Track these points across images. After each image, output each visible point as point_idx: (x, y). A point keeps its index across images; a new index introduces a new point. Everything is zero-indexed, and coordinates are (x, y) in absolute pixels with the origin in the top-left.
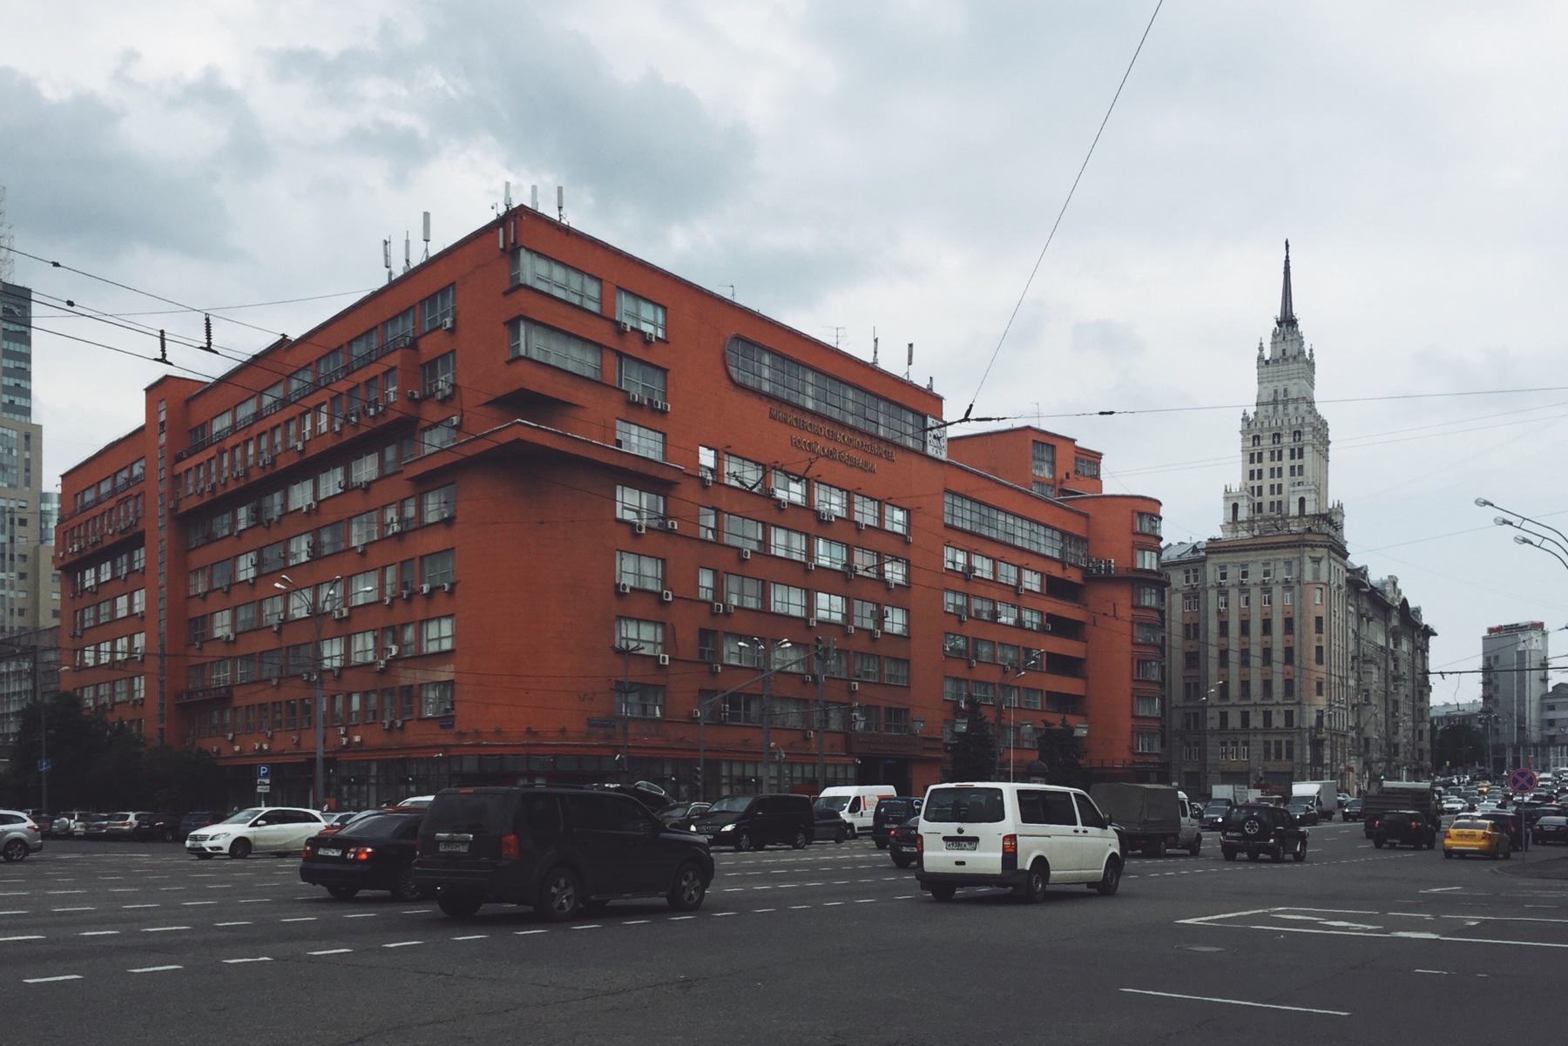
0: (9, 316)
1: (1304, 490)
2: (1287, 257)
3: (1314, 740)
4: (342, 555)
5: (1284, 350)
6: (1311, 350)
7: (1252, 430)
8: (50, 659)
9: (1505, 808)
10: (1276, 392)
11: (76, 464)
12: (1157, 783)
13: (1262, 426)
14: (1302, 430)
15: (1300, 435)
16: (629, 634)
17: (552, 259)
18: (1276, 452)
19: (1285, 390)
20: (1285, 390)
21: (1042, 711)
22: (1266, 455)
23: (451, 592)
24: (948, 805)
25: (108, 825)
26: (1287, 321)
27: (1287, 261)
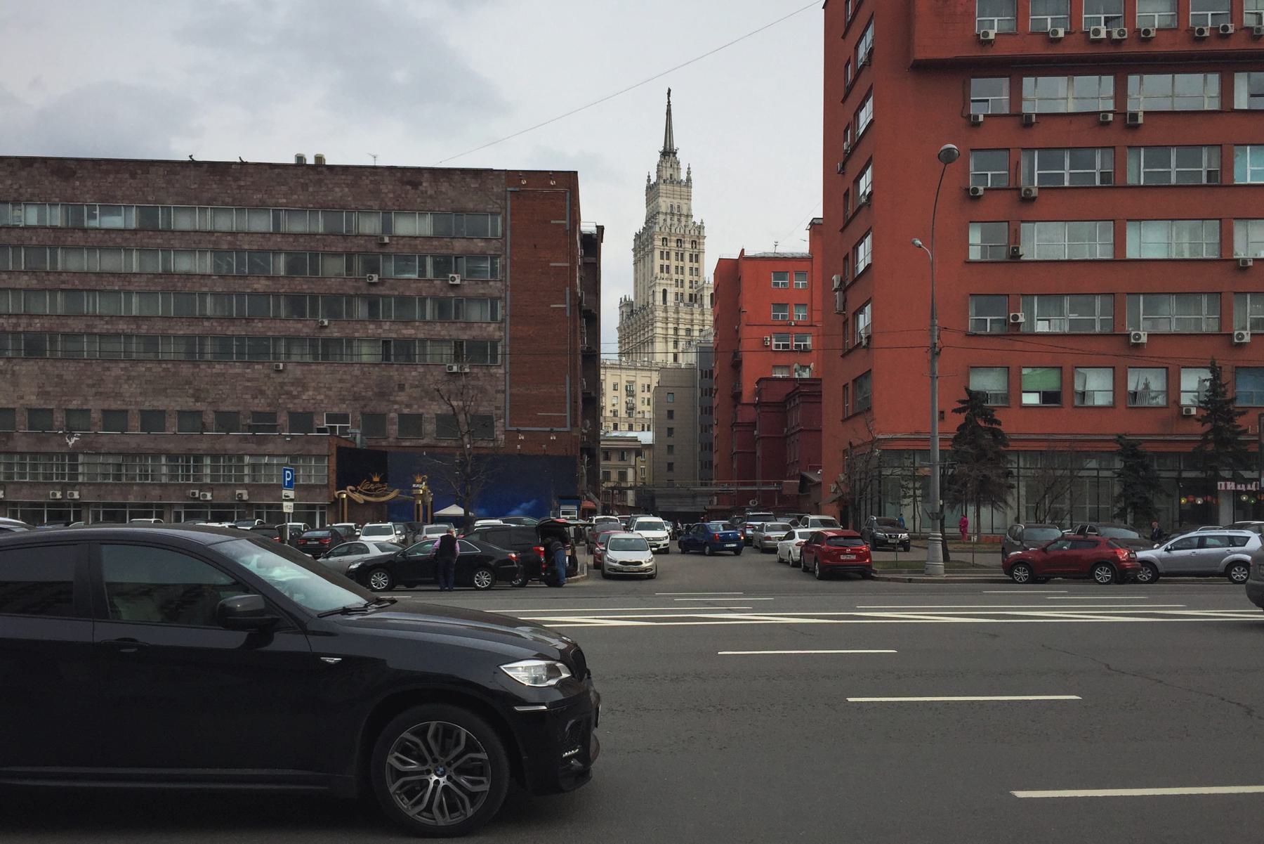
0: (415, 185)
1: (667, 284)
2: (669, 102)
3: (472, 416)
4: (985, 338)
5: (671, 175)
6: (689, 173)
7: (692, 236)
8: (1075, 401)
10: (672, 206)
12: (46, 264)
13: (699, 234)
14: (683, 239)
15: (695, 244)
17: (1064, 148)
18: (665, 253)
19: (679, 207)
20: (679, 207)
21: (1246, 293)
22: (673, 254)
23: (867, 347)
25: (57, 238)
26: (668, 153)
27: (669, 105)
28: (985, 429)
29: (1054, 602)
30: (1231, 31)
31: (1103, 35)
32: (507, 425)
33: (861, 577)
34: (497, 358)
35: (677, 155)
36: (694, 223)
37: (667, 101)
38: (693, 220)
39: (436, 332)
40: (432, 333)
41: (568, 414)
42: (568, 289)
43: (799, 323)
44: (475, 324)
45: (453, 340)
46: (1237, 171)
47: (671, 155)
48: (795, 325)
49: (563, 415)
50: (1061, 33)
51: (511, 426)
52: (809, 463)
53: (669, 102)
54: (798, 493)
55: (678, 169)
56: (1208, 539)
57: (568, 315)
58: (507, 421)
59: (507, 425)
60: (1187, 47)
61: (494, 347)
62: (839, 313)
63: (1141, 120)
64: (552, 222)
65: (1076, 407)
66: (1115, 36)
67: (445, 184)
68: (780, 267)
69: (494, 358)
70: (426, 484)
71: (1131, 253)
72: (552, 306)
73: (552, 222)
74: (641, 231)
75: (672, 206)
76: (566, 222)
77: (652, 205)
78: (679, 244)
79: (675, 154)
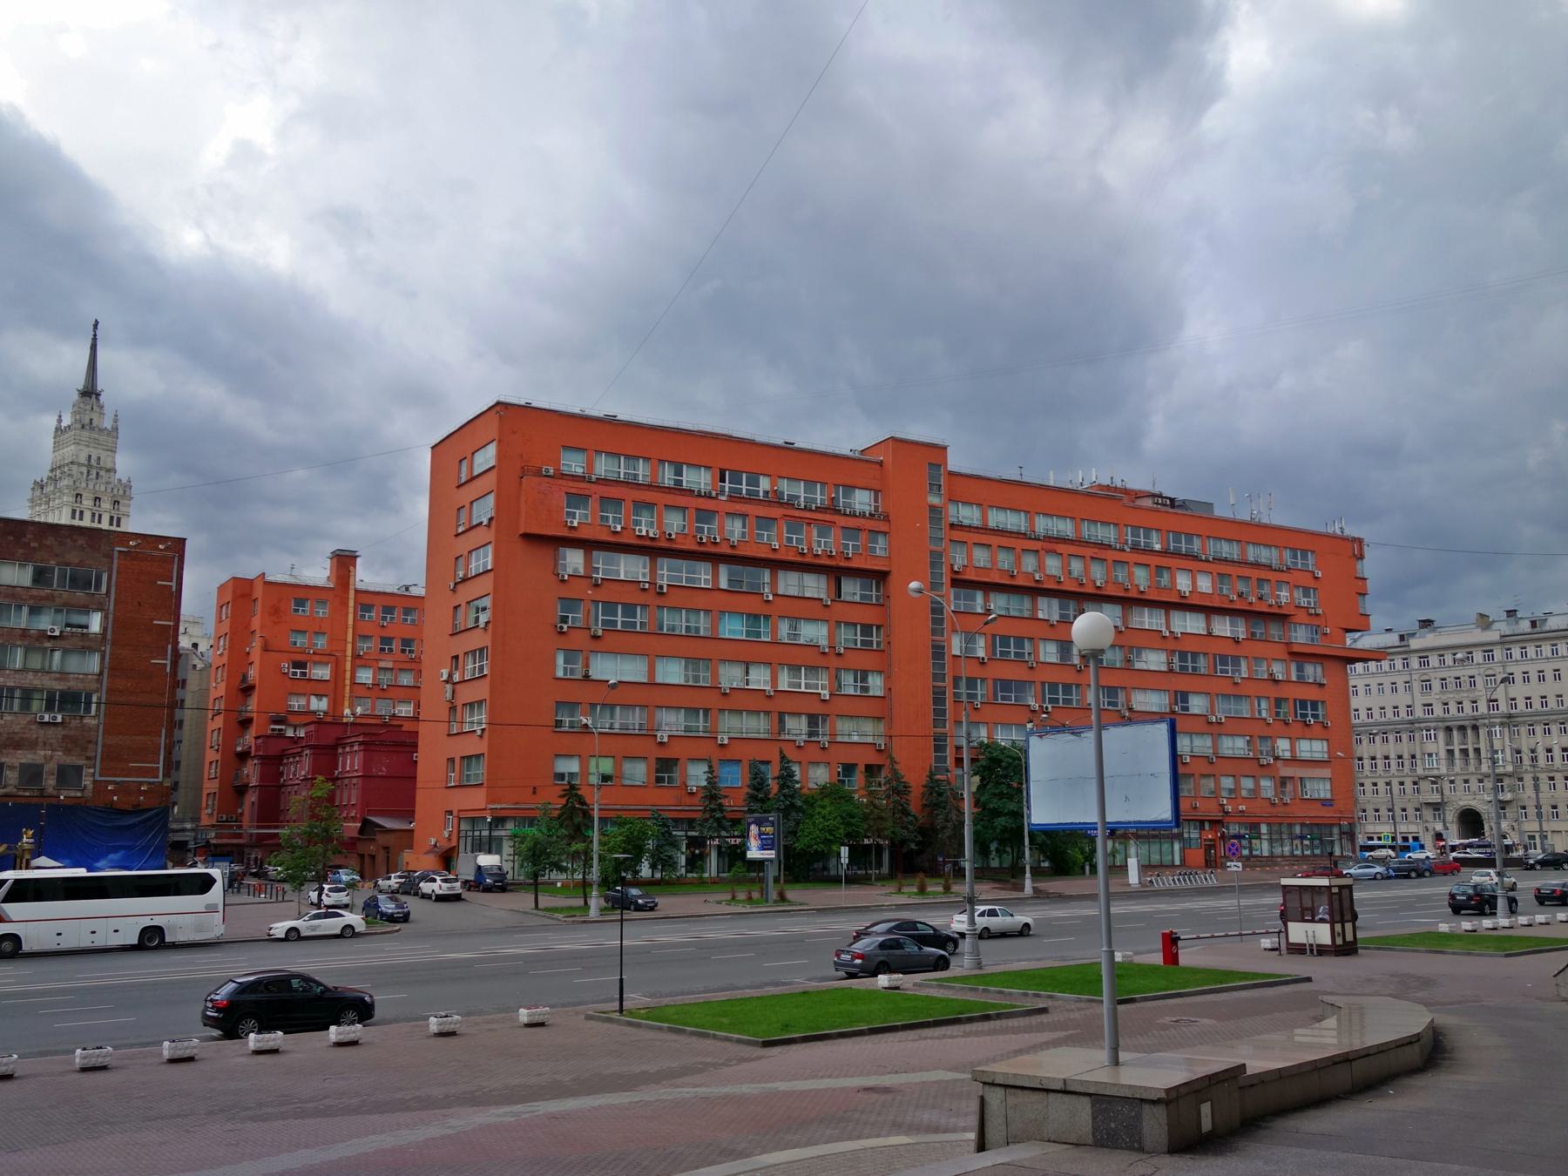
2: (95, 335)
9: (597, 478)
10: (90, 456)
11: (830, 450)
16: (1304, 902)
20: (99, 458)
24: (965, 1130)
28: (579, 809)
29: (1394, 904)
30: (718, 540)
31: (644, 533)
32: (97, 774)
33: (918, 925)
34: (90, 708)
35: (101, 398)
36: (120, 480)
37: (93, 333)
38: (118, 476)
39: (27, 681)
40: (23, 682)
41: (161, 765)
42: (170, 647)
43: (318, 652)
44: (72, 676)
45: (46, 689)
46: (721, 629)
47: (94, 396)
48: (314, 653)
49: (155, 765)
50: (619, 529)
51: (101, 776)
52: (367, 807)
53: (95, 335)
54: (357, 836)
55: (102, 414)
56: (1347, 940)
57: (168, 670)
58: (98, 770)
59: (97, 774)
60: (695, 547)
61: (88, 697)
62: (449, 701)
63: (665, 590)
64: (159, 583)
65: (954, 656)
66: (651, 535)
67: (50, 538)
68: (301, 594)
69: (88, 709)
70: (33, 836)
71: (659, 680)
72: (153, 661)
73: (159, 583)
74: (45, 481)
75: (90, 456)
76: (174, 584)
77: (61, 452)
78: (97, 503)
79: (98, 395)
